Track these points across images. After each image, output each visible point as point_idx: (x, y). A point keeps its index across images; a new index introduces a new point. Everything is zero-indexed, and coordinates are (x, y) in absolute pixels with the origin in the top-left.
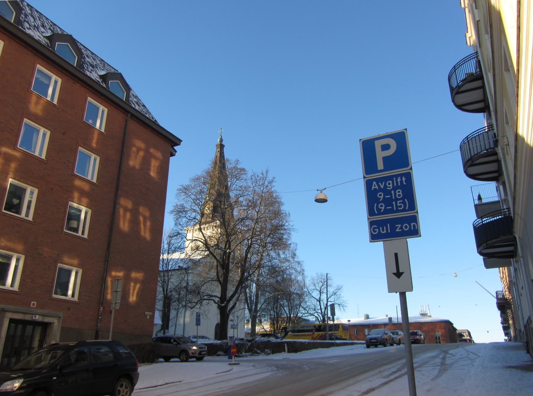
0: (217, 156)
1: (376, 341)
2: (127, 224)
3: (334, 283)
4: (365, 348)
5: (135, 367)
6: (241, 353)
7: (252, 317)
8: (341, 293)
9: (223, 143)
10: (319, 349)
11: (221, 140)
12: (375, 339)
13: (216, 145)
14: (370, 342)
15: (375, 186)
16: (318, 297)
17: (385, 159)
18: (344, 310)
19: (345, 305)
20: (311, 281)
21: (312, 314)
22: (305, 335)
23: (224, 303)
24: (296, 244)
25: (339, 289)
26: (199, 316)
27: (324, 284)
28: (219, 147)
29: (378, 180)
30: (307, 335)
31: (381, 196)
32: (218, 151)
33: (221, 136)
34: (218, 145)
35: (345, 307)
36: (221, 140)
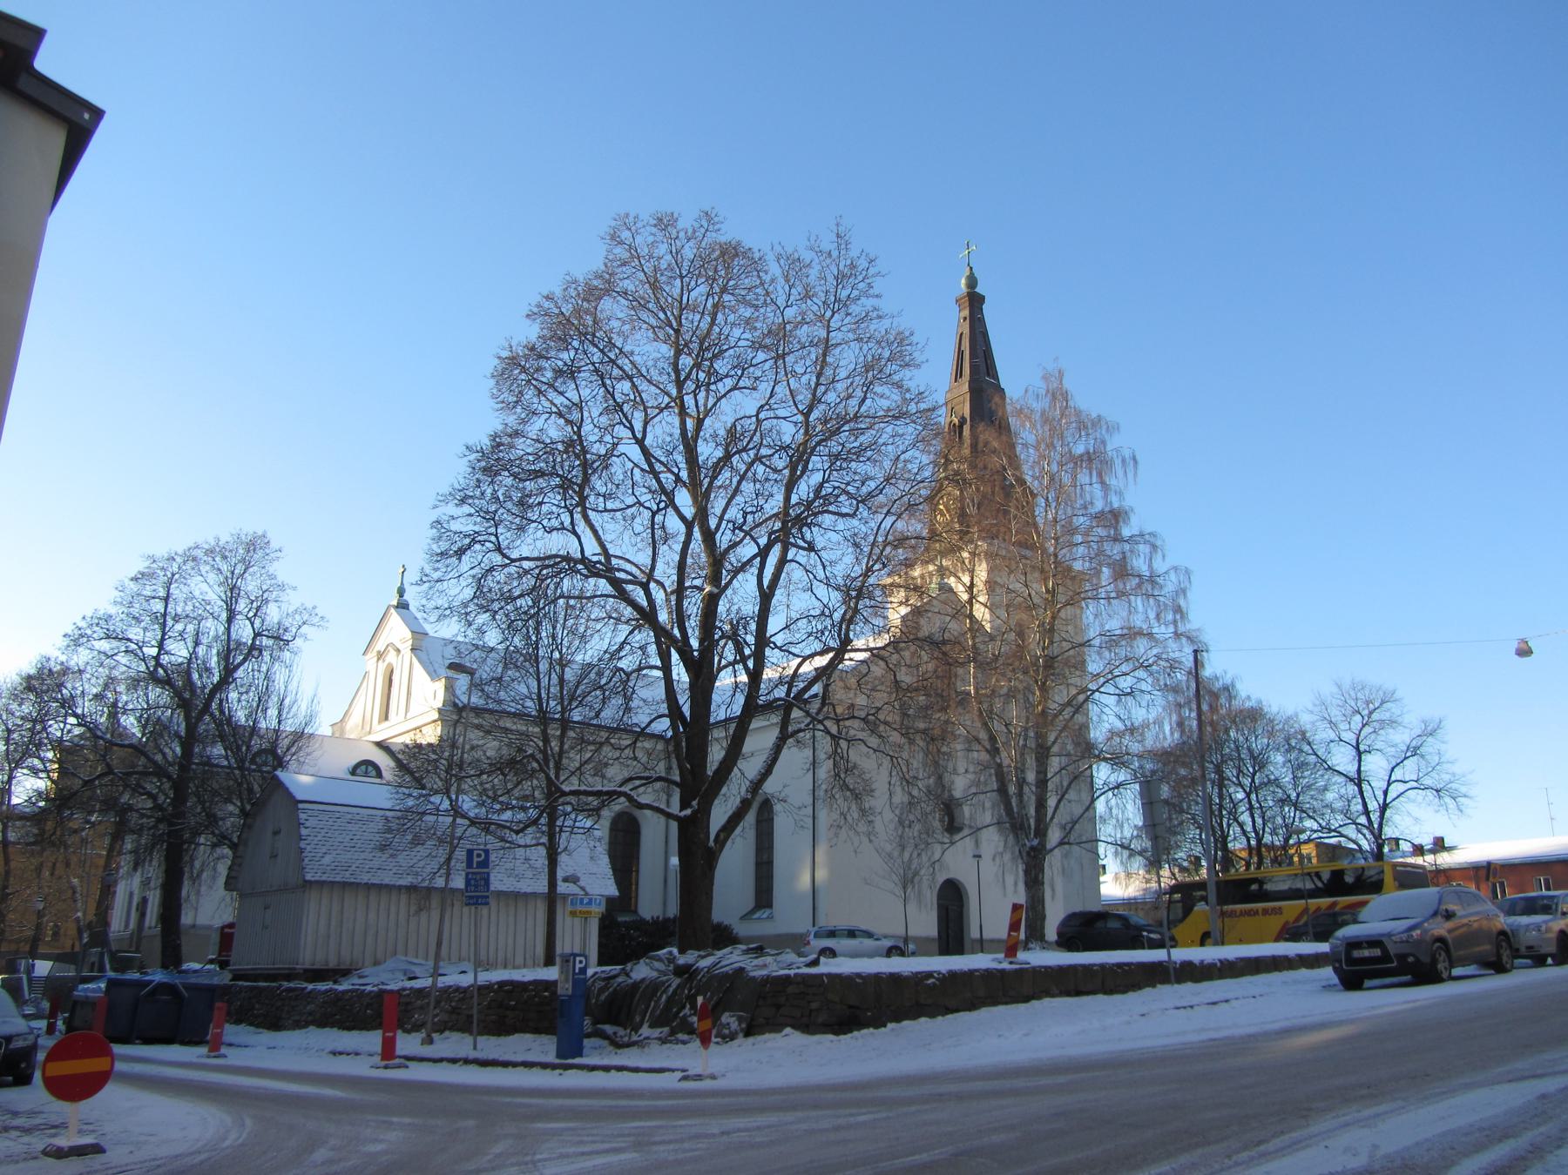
0: (961, 334)
1: (1377, 952)
3: (1412, 713)
4: (1328, 987)
5: (1173, 978)
6: (636, 1029)
7: (1024, 854)
8: (1443, 747)
10: (1047, 1001)
11: (972, 282)
12: (1374, 942)
13: (957, 301)
14: (1351, 961)
16: (1351, 769)
17: (478, 862)
18: (1461, 811)
19: (1463, 790)
20: (1316, 709)
21: (1335, 831)
22: (1256, 913)
23: (690, 806)
24: (1188, 572)
25: (1430, 731)
26: (485, 864)
27: (1369, 718)
28: (967, 304)
29: (473, 873)
30: (1260, 911)
31: (473, 882)
32: (965, 319)
33: (971, 268)
34: (962, 299)
35: (1465, 796)
36: (972, 282)
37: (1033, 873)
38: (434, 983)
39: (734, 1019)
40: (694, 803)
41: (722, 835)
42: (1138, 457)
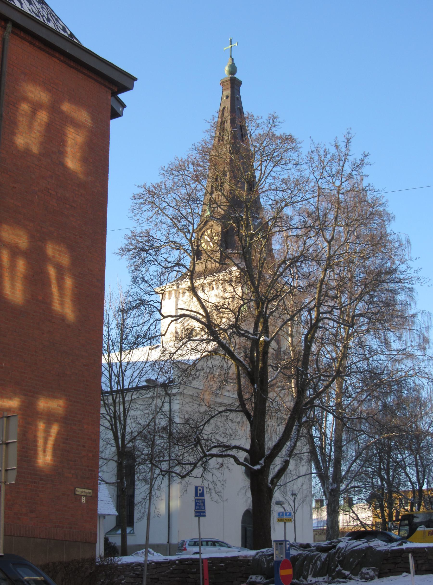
0: (224, 108)
2: (19, 286)
7: (327, 494)
9: (237, 76)
11: (233, 70)
13: (222, 83)
15: (197, 501)
17: (200, 493)
26: (202, 495)
29: (198, 499)
31: (198, 504)
32: (227, 97)
33: (233, 59)
34: (225, 82)
36: (233, 70)
37: (333, 505)
38: (146, 560)
39: (371, 570)
40: (262, 462)
41: (275, 480)
42: (411, 241)
